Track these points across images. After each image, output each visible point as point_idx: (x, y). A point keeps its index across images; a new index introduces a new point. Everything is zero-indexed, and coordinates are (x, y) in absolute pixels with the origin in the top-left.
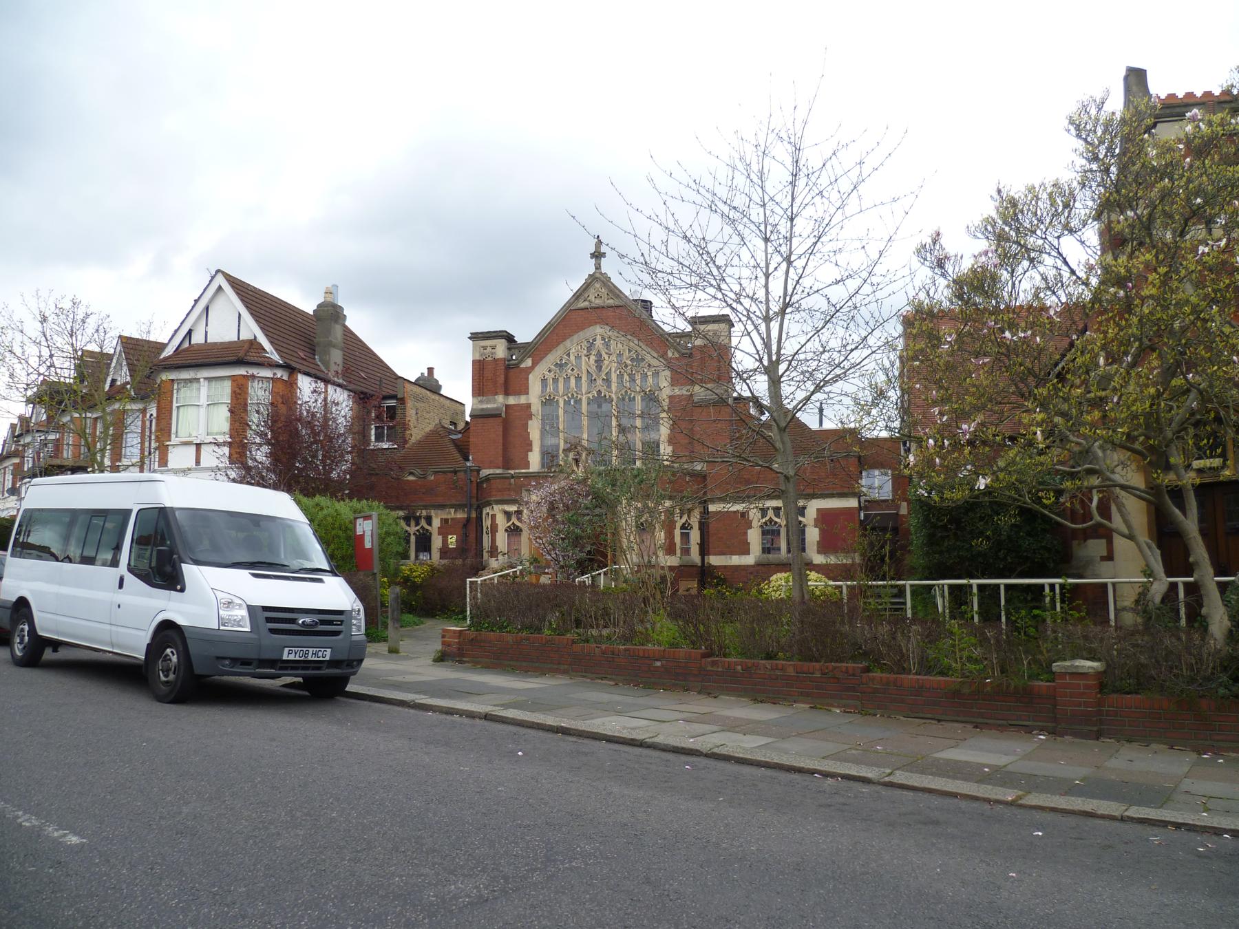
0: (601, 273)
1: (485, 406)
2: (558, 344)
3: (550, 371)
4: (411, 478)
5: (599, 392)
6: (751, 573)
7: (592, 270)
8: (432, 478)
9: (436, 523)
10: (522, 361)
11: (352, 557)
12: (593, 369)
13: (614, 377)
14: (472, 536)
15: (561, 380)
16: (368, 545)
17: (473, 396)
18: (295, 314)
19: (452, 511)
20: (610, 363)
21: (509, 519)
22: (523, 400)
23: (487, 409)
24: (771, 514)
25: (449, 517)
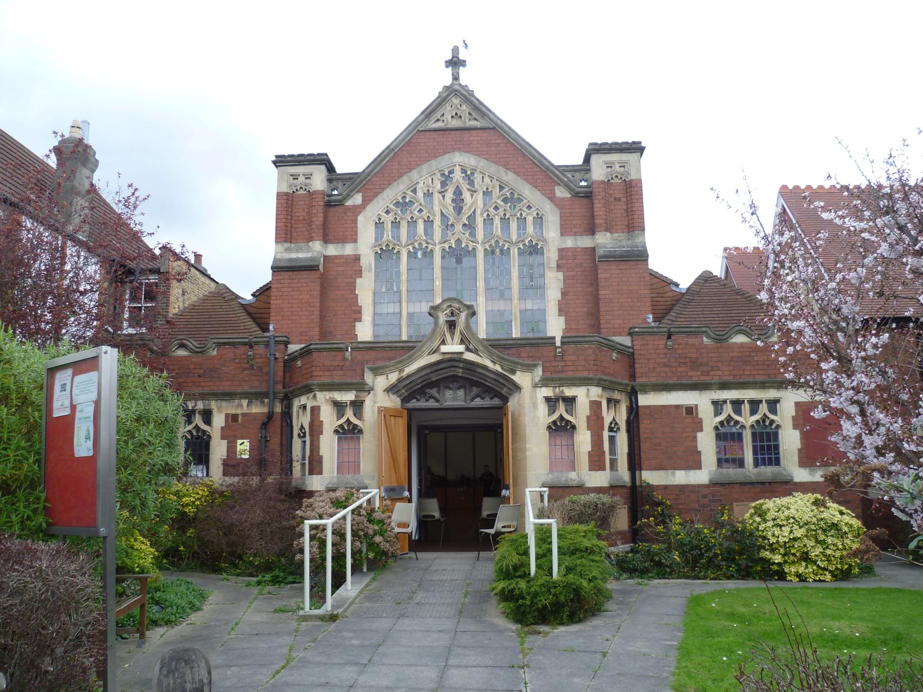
0: (460, 85)
1: (294, 256)
2: (401, 176)
3: (387, 212)
4: (182, 353)
5: (459, 241)
6: (705, 496)
7: (448, 81)
8: (215, 353)
9: (219, 420)
10: (348, 196)
11: (33, 485)
12: (450, 211)
13: (479, 221)
14: (275, 440)
15: (404, 224)
16: (82, 447)
17: (277, 241)
18: (26, 155)
19: (245, 402)
20: (474, 202)
21: (340, 414)
22: (348, 250)
23: (297, 259)
24: (728, 410)
25: (239, 411)
